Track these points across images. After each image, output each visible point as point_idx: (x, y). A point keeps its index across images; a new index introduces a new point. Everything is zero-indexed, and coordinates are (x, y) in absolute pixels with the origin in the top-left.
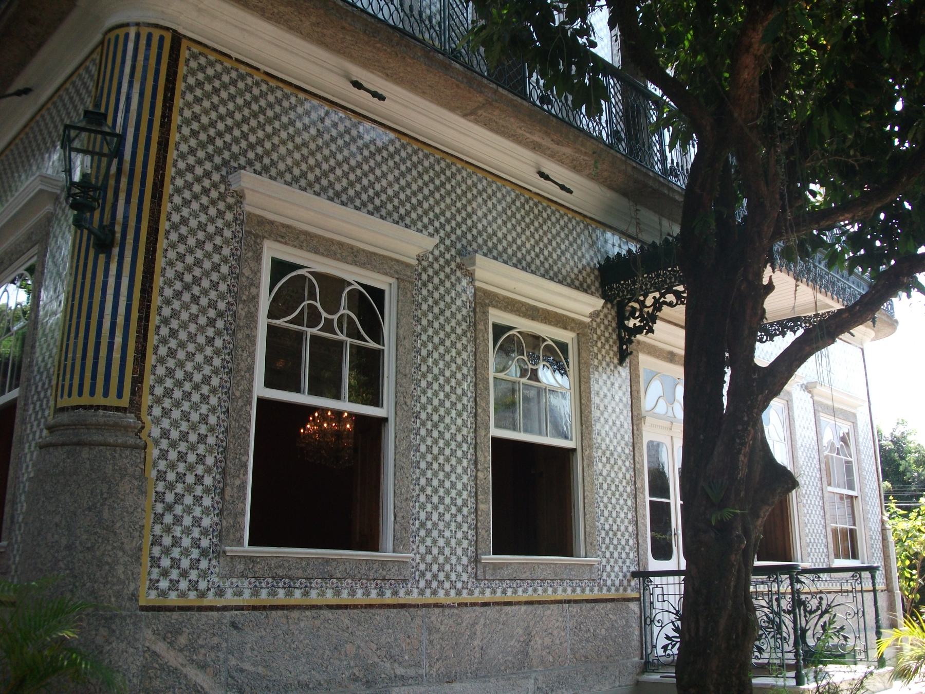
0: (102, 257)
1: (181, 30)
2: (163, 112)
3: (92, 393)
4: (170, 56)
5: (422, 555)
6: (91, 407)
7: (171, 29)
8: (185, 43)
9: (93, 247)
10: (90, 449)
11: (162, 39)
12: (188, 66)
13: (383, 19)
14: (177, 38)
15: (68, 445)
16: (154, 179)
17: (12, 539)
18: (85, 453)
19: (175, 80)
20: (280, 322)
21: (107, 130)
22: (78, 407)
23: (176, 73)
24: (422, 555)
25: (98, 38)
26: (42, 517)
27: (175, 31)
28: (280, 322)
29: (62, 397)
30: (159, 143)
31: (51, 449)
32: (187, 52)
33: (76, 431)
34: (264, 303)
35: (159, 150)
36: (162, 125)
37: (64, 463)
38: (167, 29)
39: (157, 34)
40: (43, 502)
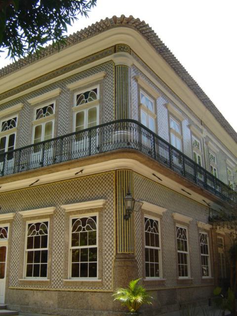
20: (74, 232)
28: (74, 232)
34: (71, 229)
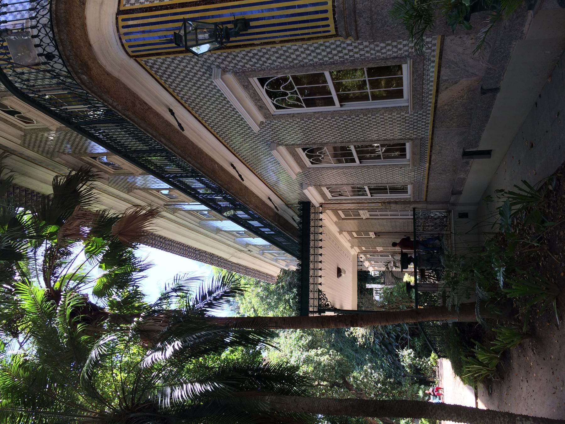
0: (252, 24)
1: (116, 11)
2: (165, 9)
3: (327, 19)
4: (132, 13)
5: (391, 44)
6: (334, 10)
7: (116, 17)
8: (122, 8)
9: (247, 31)
10: (357, 4)
11: (123, 20)
12: (135, 4)
13: (49, 13)
14: (120, 12)
15: (356, 18)
16: (204, 5)
17: (406, 55)
18: (359, 6)
19: (145, 8)
21: (182, 33)
22: (334, 18)
23: (141, 9)
24: (391, 44)
25: (132, 62)
26: (396, 25)
27: (117, 14)
29: (329, 31)
30: (183, 7)
31: (359, 29)
32: (126, 5)
33: (347, 16)
35: (187, 6)
36: (172, 8)
37: (365, 18)
38: (117, 18)
39: (121, 24)
40: (387, 26)
